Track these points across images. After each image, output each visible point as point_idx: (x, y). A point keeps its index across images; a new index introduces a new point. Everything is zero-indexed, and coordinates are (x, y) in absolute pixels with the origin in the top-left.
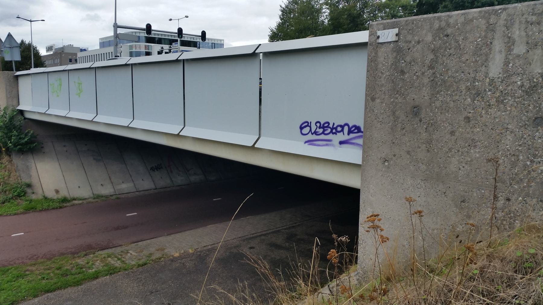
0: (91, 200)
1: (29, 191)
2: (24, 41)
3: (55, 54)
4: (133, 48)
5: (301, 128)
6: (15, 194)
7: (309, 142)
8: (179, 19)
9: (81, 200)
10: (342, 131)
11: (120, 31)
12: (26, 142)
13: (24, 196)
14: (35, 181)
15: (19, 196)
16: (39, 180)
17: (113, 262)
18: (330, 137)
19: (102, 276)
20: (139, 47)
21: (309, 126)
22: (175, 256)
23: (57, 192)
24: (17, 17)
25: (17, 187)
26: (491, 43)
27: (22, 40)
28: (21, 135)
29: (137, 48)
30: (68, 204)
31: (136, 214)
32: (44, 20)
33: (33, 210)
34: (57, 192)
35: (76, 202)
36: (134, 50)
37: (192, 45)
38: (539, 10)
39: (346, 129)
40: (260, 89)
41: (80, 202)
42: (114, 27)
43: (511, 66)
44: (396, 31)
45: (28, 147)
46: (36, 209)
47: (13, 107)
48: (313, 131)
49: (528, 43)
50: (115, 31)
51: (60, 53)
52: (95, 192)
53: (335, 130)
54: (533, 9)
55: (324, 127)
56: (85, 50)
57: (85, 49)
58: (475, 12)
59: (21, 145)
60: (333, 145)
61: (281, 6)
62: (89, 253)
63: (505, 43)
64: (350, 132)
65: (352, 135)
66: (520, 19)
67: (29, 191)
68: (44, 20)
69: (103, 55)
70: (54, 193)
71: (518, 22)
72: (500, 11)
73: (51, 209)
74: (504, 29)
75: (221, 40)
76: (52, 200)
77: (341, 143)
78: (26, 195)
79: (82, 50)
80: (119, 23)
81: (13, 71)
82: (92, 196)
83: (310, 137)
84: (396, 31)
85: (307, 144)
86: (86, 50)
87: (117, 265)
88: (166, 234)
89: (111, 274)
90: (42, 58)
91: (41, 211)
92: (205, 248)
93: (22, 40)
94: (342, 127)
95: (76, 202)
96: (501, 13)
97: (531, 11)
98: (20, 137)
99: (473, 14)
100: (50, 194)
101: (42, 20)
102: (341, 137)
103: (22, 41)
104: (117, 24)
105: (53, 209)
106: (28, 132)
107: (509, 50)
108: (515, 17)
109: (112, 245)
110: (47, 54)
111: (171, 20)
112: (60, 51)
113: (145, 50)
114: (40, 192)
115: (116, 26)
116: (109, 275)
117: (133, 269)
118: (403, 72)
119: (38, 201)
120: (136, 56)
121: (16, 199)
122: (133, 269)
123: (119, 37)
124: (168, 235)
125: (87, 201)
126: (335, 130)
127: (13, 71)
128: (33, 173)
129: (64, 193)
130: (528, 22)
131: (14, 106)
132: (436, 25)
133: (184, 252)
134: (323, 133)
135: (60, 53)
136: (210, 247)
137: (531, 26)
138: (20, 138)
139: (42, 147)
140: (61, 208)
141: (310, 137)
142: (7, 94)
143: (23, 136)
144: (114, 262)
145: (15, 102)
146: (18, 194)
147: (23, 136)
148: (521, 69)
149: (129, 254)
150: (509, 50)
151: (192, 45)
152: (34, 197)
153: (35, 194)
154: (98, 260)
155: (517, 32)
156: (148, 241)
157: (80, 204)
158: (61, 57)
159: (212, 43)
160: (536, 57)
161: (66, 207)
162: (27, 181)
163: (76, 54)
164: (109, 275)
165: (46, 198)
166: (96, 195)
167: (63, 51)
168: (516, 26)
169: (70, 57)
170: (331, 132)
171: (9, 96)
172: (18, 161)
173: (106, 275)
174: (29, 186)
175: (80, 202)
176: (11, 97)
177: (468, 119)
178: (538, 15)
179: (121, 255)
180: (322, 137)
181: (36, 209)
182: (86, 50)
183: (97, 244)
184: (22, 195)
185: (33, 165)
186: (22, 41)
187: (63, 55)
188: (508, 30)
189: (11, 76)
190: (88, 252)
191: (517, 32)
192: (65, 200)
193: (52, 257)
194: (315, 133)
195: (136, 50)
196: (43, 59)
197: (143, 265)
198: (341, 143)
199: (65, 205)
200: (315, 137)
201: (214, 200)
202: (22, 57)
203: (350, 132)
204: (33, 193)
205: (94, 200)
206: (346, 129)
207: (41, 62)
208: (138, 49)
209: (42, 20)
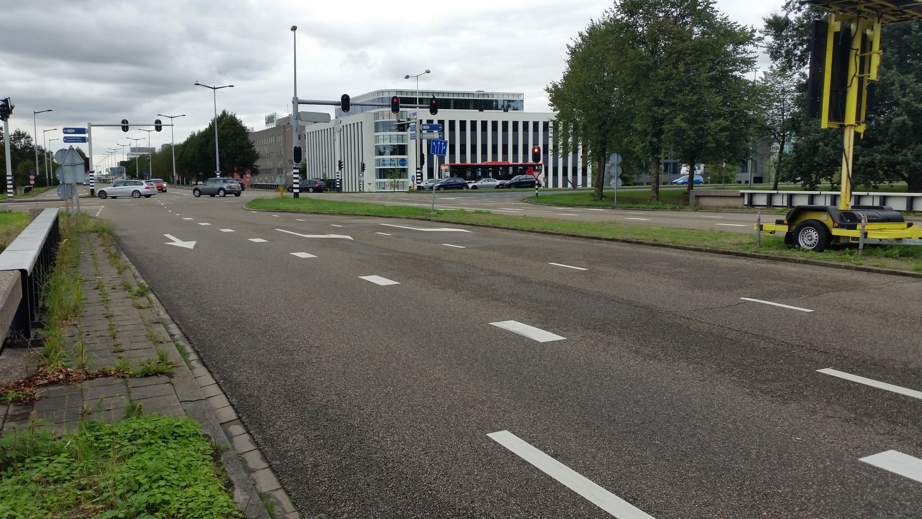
2: (227, 112)
3: (278, 127)
4: (379, 117)
8: (417, 76)
11: (302, 108)
20: (388, 115)
24: (196, 84)
27: (224, 110)
32: (233, 86)
36: (381, 120)
37: (471, 105)
42: (293, 103)
50: (295, 108)
51: (284, 126)
61: (568, 47)
68: (233, 86)
69: (352, 125)
75: (519, 95)
80: (301, 97)
81: (419, 98)
93: (224, 110)
101: (230, 86)
103: (224, 112)
104: (297, 98)
110: (267, 128)
111: (407, 77)
115: (297, 102)
120: (455, 108)
123: (301, 118)
127: (419, 98)
151: (471, 105)
158: (284, 132)
159: (504, 100)
186: (224, 112)
187: (288, 130)
190: (700, 434)
195: (384, 120)
196: (251, 139)
201: (505, 439)
202: (841, 29)
209: (230, 86)
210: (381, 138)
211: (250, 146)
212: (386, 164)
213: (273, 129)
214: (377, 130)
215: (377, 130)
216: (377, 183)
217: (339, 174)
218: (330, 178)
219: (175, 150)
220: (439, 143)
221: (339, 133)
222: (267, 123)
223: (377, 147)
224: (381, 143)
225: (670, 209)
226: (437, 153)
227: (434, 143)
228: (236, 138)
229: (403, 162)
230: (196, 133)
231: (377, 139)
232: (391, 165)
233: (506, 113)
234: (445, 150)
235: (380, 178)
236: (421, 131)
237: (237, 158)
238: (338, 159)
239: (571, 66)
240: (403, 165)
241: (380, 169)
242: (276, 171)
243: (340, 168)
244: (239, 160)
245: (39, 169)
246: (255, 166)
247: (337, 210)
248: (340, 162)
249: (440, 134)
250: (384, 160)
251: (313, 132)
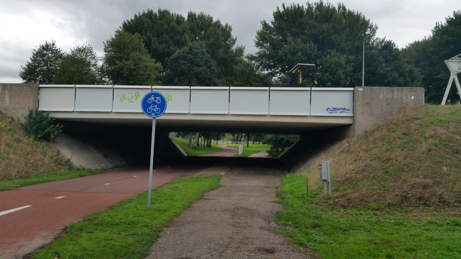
5: (327, 110)
7: (330, 113)
10: (341, 109)
18: (337, 111)
39: (342, 109)
43: (39, 70)
44: (363, 89)
48: (331, 110)
53: (338, 109)
55: (335, 109)
58: (422, 98)
60: (338, 113)
64: (343, 110)
65: (343, 110)
77: (340, 112)
83: (330, 112)
84: (363, 89)
94: (341, 109)
102: (340, 111)
107: (383, 93)
118: (364, 96)
126: (338, 109)
132: (371, 89)
134: (335, 110)
141: (330, 112)
170: (337, 110)
177: (377, 104)
180: (334, 111)
194: (332, 110)
198: (340, 112)
200: (332, 111)
203: (343, 110)
206: (342, 109)
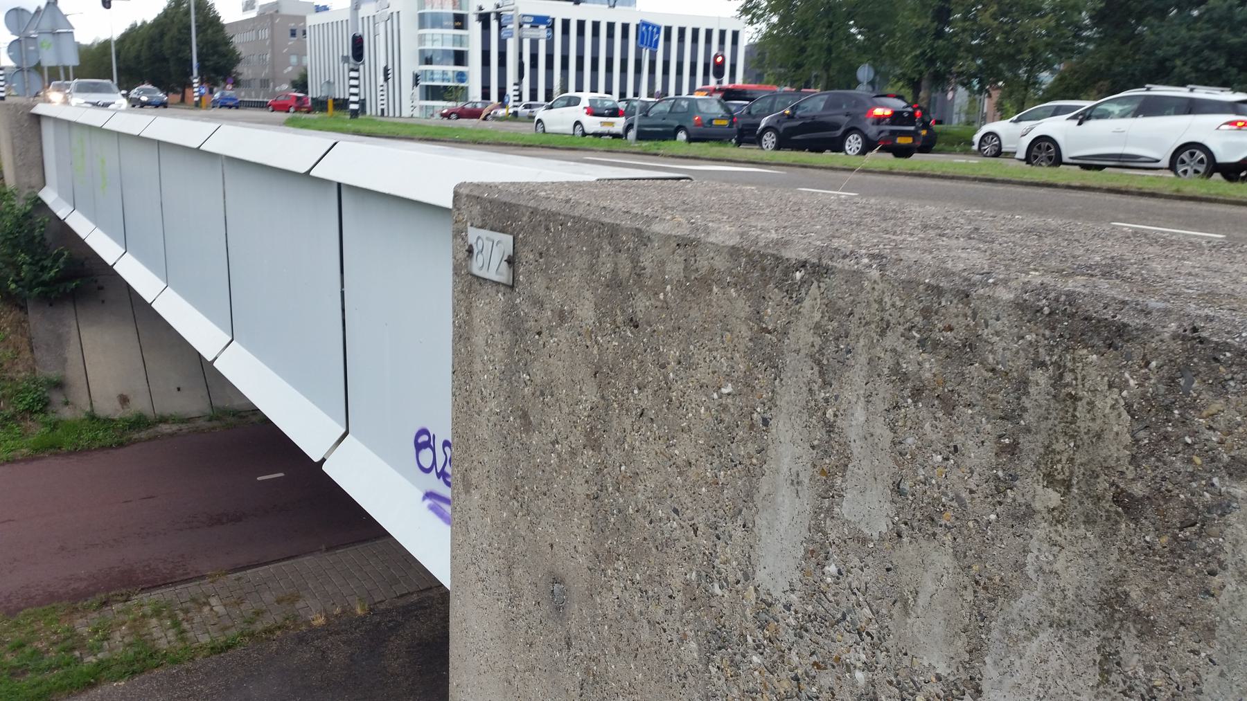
0: (204, 423)
1: (56, 397)
3: (261, 16)
6: (21, 407)
9: (174, 422)
12: (51, 278)
13: (41, 411)
14: (73, 373)
15: (30, 411)
16: (84, 371)
17: (157, 633)
19: (109, 678)
21: (430, 447)
22: (315, 623)
23: (124, 400)
25: (28, 390)
26: (766, 422)
28: (45, 259)
29: (435, 5)
30: (143, 435)
31: (281, 475)
33: (52, 450)
34: (124, 400)
35: (165, 428)
38: (951, 329)
40: (342, 293)
41: (175, 428)
45: (61, 290)
46: (60, 448)
47: (30, 190)
49: (898, 489)
52: (217, 403)
54: (926, 313)
56: (325, 8)
57: (325, 6)
59: (43, 284)
62: (115, 598)
63: (813, 447)
66: (872, 346)
67: (56, 397)
70: (117, 404)
71: (863, 359)
72: (798, 275)
73: (95, 449)
74: (810, 372)
76: (108, 422)
78: (49, 408)
79: (318, 9)
82: (208, 411)
85: (428, 502)
86: (328, 9)
87: (162, 645)
88: (323, 547)
89: (134, 673)
90: (226, 28)
91: (70, 453)
92: (400, 602)
95: (165, 428)
96: (803, 282)
97: (919, 320)
98: (42, 265)
99: (712, 254)
100: (107, 406)
105: (103, 448)
106: (60, 254)
108: (853, 325)
109: (183, 575)
112: (271, 12)
113: (454, 9)
114: (83, 402)
116: (127, 678)
117: (197, 659)
119: (73, 427)
121: (24, 418)
122: (197, 659)
124: (328, 550)
125: (190, 425)
128: (72, 354)
129: (140, 405)
130: (905, 377)
131: (33, 187)
133: (343, 612)
135: (271, 16)
136: (415, 598)
137: (915, 402)
138: (43, 269)
139: (101, 288)
140: (121, 445)
142: (14, 159)
143: (48, 263)
144: (162, 636)
145: (35, 179)
146: (27, 407)
147: (48, 263)
148: (867, 611)
149: (206, 609)
150: (829, 494)
152: (67, 414)
153: (71, 406)
154: (124, 623)
155: (860, 415)
156: (271, 568)
157: (172, 435)
160: (929, 586)
161: (139, 441)
162: (53, 374)
163: (303, 19)
164: (127, 678)
165: (92, 417)
166: (218, 408)
167: (277, 11)
168: (857, 374)
169: (292, 25)
171: (20, 164)
172: (39, 322)
173: (121, 678)
174: (59, 385)
175: (175, 428)
176: (24, 165)
178: (943, 352)
179: (186, 611)
181: (60, 448)
182: (328, 9)
183: (147, 569)
184: (38, 409)
185: (74, 332)
188: (826, 384)
189: (23, 113)
190: (113, 596)
191: (860, 415)
192: (139, 422)
193: (22, 605)
196: (228, 32)
197: (222, 650)
199: (136, 436)
202: (80, 61)
204: (67, 403)
205: (209, 425)
207: (224, 38)
208: (438, 8)
210: (428, 37)
211: (227, 42)
212: (437, 79)
213: (253, 19)
214: (422, 25)
215: (422, 25)
216: (421, 107)
217: (385, 88)
218: (342, 97)
219: (198, 27)
220: (650, 28)
221: (383, 23)
222: (245, 10)
223: (422, 52)
224: (428, 46)
225: (961, 151)
226: (650, 46)
227: (644, 28)
228: (207, 29)
229: (461, 77)
230: (139, 24)
231: (422, 39)
232: (443, 80)
233: (612, 9)
234: (657, 41)
235: (427, 99)
236: (521, 26)
237: (208, 60)
238: (381, 64)
239: (141, 26)
240: (463, 81)
241: (427, 86)
242: (258, 83)
243: (386, 79)
244: (211, 63)
245: (190, 20)
246: (235, 72)
247: (407, 132)
248: (386, 70)
249: (548, 32)
250: (432, 73)
251: (337, 22)
